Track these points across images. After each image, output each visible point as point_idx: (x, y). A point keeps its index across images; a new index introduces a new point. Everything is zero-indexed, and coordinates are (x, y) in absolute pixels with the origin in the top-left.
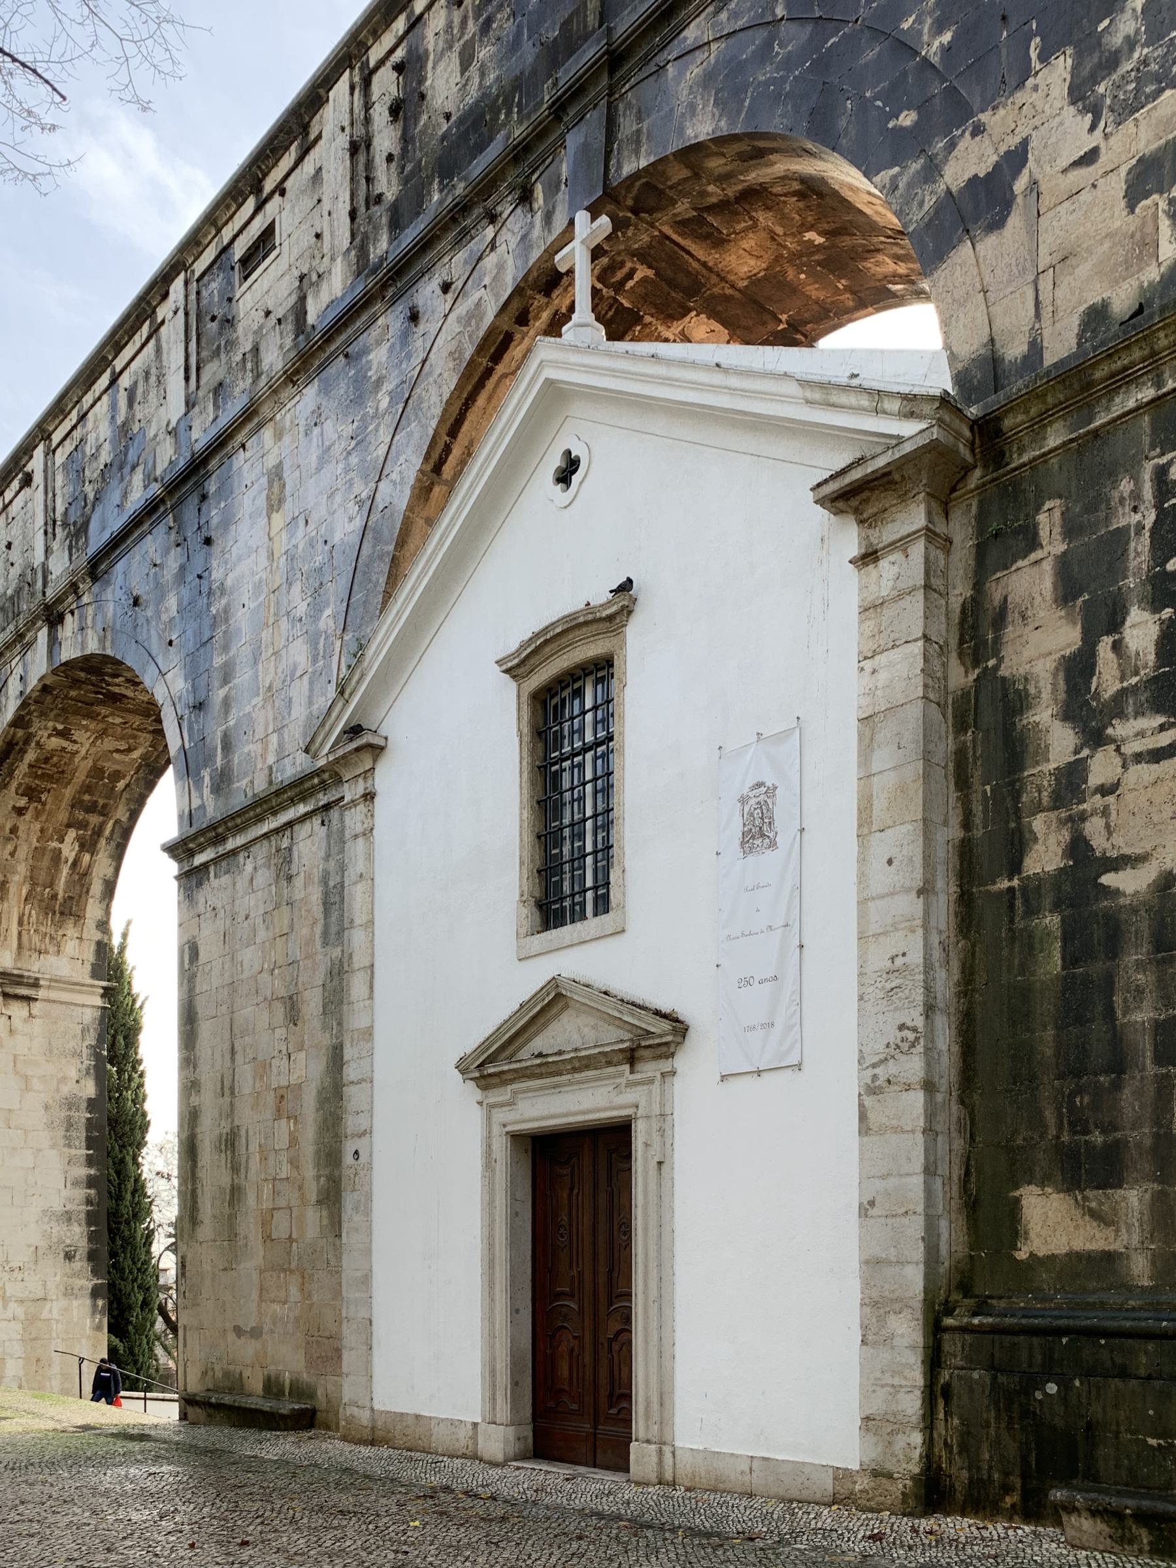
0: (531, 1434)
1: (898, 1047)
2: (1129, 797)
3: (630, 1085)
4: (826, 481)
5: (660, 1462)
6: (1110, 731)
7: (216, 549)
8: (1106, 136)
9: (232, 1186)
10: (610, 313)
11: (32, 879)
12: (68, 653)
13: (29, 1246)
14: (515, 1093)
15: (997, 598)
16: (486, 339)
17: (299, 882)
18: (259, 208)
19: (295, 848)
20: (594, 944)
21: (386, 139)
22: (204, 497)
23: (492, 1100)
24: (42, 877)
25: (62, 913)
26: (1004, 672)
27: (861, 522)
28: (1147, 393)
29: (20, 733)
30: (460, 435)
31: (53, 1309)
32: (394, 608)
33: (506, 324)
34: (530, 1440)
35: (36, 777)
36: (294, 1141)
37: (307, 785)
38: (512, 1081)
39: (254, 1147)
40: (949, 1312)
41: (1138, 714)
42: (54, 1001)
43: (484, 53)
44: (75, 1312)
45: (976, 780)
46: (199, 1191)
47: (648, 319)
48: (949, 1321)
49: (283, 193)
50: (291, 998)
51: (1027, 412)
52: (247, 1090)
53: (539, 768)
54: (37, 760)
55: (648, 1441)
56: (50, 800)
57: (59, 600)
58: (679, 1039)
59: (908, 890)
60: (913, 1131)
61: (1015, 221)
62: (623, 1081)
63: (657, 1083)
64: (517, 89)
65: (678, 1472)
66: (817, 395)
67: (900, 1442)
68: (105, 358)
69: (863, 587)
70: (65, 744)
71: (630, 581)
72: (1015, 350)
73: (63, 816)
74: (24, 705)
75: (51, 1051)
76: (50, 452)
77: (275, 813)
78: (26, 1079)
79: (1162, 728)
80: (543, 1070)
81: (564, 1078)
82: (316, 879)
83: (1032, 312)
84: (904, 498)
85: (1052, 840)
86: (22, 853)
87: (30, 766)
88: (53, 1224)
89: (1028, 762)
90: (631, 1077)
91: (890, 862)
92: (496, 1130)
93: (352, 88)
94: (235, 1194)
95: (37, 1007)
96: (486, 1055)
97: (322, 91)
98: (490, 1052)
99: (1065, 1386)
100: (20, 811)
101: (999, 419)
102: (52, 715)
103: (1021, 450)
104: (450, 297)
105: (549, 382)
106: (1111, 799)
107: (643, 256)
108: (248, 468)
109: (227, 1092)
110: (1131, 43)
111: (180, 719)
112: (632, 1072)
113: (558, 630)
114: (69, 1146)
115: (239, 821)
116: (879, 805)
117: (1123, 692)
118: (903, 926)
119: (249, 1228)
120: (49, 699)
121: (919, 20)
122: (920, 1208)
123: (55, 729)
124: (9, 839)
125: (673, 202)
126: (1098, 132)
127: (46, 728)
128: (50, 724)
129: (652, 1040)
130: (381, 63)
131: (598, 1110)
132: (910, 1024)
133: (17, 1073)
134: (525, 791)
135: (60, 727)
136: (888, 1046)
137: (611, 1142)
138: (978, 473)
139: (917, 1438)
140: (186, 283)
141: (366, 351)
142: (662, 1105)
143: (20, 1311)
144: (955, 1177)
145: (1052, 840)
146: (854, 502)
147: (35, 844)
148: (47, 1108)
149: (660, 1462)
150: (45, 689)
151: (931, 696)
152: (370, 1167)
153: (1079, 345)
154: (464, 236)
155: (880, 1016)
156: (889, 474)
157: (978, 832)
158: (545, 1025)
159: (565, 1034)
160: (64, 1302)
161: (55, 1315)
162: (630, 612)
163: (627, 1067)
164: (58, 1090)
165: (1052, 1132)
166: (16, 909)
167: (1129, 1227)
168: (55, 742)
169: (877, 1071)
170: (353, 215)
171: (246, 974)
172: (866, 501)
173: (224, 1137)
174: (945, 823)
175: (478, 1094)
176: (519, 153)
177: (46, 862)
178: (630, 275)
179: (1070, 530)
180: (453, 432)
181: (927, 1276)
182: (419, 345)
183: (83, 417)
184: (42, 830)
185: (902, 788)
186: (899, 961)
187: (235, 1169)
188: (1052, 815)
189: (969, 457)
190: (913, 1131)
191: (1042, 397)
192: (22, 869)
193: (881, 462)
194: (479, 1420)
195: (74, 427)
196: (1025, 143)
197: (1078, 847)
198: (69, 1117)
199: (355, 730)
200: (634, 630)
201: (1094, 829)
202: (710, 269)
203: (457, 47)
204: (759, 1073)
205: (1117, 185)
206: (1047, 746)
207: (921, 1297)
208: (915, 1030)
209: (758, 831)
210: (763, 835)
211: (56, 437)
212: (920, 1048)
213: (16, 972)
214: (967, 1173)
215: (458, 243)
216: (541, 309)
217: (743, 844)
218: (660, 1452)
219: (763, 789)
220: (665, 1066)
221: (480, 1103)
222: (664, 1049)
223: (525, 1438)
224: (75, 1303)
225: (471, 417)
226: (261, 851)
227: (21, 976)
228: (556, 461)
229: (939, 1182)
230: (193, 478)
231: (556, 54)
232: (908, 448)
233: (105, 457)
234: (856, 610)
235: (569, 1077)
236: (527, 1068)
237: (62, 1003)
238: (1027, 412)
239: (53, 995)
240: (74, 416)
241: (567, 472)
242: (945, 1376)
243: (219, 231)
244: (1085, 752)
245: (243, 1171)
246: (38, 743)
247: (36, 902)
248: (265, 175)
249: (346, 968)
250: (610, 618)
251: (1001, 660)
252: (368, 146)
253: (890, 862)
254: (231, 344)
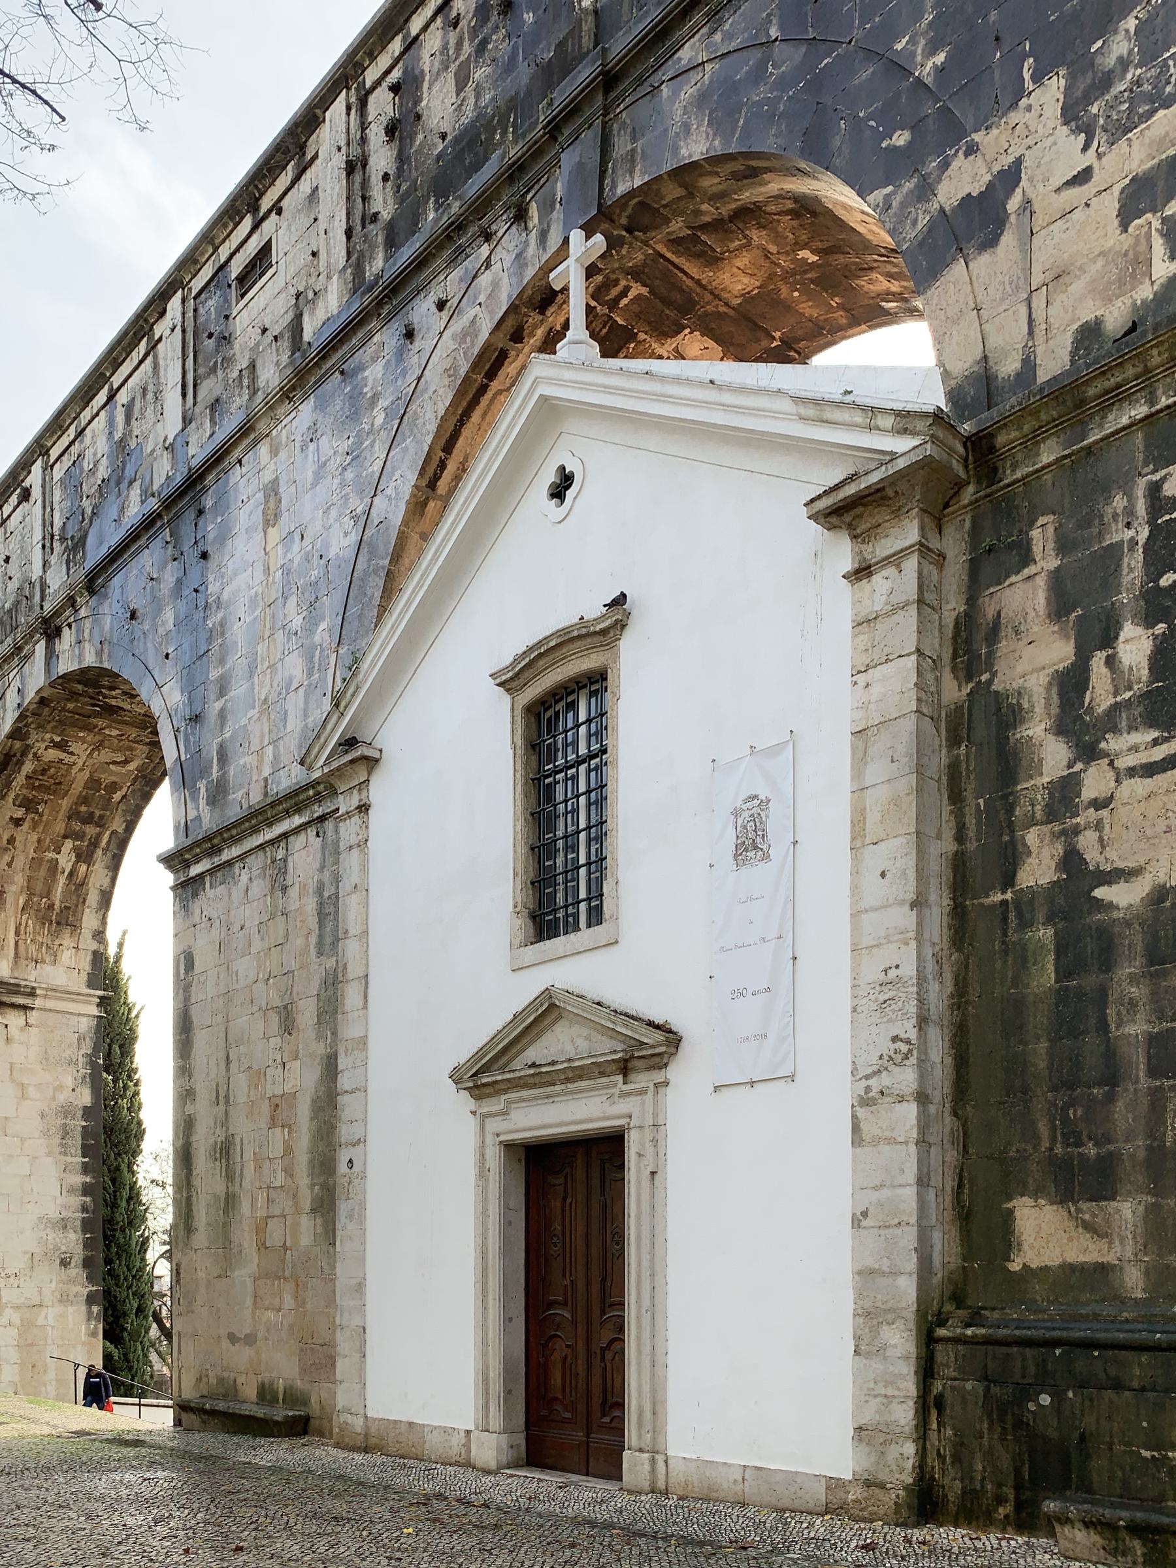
0: (523, 1443)
1: (891, 1058)
2: (1122, 811)
3: (623, 1095)
4: (819, 497)
5: (653, 1470)
6: (1103, 745)
7: (212, 563)
8: (1100, 156)
9: (227, 1193)
10: (604, 331)
11: (29, 889)
12: (66, 665)
13: (25, 1253)
14: (508, 1102)
15: (990, 613)
16: (480, 356)
17: (293, 892)
18: (256, 227)
19: (290, 859)
20: (603, 950)
21: (382, 159)
22: (201, 512)
23: (485, 1110)
24: (39, 886)
25: (58, 923)
26: (997, 686)
27: (855, 537)
28: (1140, 410)
29: (18, 744)
30: (455, 451)
31: (49, 1316)
32: (390, 621)
33: (502, 342)
34: (523, 1449)
35: (34, 788)
36: (288, 1150)
37: (301, 797)
38: (505, 1091)
39: (248, 1155)
40: (942, 1323)
41: (1132, 728)
42: (50, 1010)
43: (479, 74)
44: (70, 1318)
45: (969, 794)
47: (642, 336)
48: (942, 1332)
49: (279, 213)
50: (285, 1007)
51: (1020, 428)
52: (241, 1099)
53: (533, 780)
54: (35, 771)
55: (641, 1450)
56: (47, 812)
57: (57, 613)
58: (672, 1050)
59: (901, 903)
60: (906, 1143)
61: (1008, 240)
62: (616, 1091)
63: (650, 1094)
64: (513, 108)
65: (671, 1481)
66: (811, 412)
67: (893, 1452)
68: (102, 374)
69: (857, 602)
70: (62, 755)
71: (623, 596)
72: (1008, 367)
73: (60, 827)
74: (21, 717)
75: (47, 1059)
76: (49, 467)
77: (270, 825)
78: (23, 1087)
79: (1156, 742)
80: (537, 1080)
81: (557, 1088)
82: (311, 891)
83: (1025, 330)
84: (897, 513)
85: (1046, 852)
86: (20, 862)
87: (28, 777)
88: (48, 1231)
89: (1022, 775)
90: (625, 1087)
91: (883, 875)
92: (490, 1139)
93: (349, 108)
94: (230, 1202)
95: (33, 1016)
96: (479, 1065)
97: (318, 112)
98: (484, 1061)
99: (1058, 1397)
100: (17, 822)
101: (992, 436)
102: (49, 727)
103: (1014, 467)
104: (445, 314)
105: (544, 399)
106: (1104, 813)
107: (637, 274)
108: (244, 483)
109: (222, 1101)
110: (1124, 64)
111: (177, 731)
112: (625, 1083)
113: (552, 644)
114: (65, 1154)
115: (234, 832)
116: (873, 817)
117: (1116, 706)
118: (895, 938)
120: (46, 711)
121: (913, 41)
122: (913, 1220)
123: (52, 741)
124: (6, 849)
125: (668, 221)
126: (1092, 151)
127: (43, 740)
128: (48, 736)
129: (645, 1050)
130: (377, 83)
131: (591, 1120)
132: (903, 1036)
133: (13, 1081)
134: (519, 803)
135: (57, 739)
136: (881, 1057)
137: (605, 1151)
138: (971, 489)
139: (910, 1449)
140: (183, 301)
141: (361, 368)
142: (655, 1115)
143: (16, 1317)
144: (948, 1189)
145: (1046, 852)
146: (848, 518)
147: (32, 854)
148: (43, 1116)
149: (653, 1470)
150: (42, 701)
151: (925, 711)
152: (363, 1176)
153: (1072, 362)
154: (460, 254)
155: (874, 1029)
156: (883, 488)
157: (972, 846)
158: (539, 1035)
159: (560, 1044)
160: (59, 1309)
161: (51, 1321)
162: (623, 627)
163: (620, 1078)
164: (54, 1099)
165: (1046, 1144)
166: (13, 919)
167: (1123, 1240)
168: (53, 754)
169: (870, 1082)
170: (349, 233)
171: (242, 984)
172: (860, 516)
173: (219, 1144)
174: (939, 837)
175: (472, 1104)
176: (515, 172)
177: (43, 872)
178: (624, 294)
179: (1064, 546)
180: (448, 448)
181: (920, 1288)
182: (414, 362)
183: (80, 433)
184: (39, 841)
185: (896, 802)
186: (892, 974)
187: (230, 1176)
188: (1046, 829)
189: (962, 474)
190: (906, 1143)
191: (1035, 413)
192: (19, 879)
193: (874, 478)
194: (472, 1428)
195: (72, 443)
196: (1018, 162)
197: (1071, 861)
198: (65, 1126)
199: (350, 743)
200: (628, 644)
201: (1087, 843)
202: (704, 287)
203: (453, 67)
204: (752, 1084)
205: (1110, 204)
206: (1041, 760)
207: (914, 1308)
208: (908, 1042)
209: (751, 844)
210: (756, 848)
211: (54, 453)
212: (913, 1060)
213: (12, 981)
214: (960, 1185)
215: (453, 261)
216: (536, 326)
217: (736, 856)
218: (653, 1461)
219: (757, 802)
220: (658, 1076)
221: (474, 1113)
222: (657, 1060)
223: (518, 1446)
224: (71, 1309)
225: (466, 432)
226: (256, 862)
227: (18, 985)
228: (549, 477)
229: (932, 1194)
230: (190, 493)
231: (551, 74)
232: (901, 464)
233: (103, 472)
234: (850, 625)
235: (562, 1087)
236: (520, 1078)
237: (58, 1012)
238: (1020, 428)
239: (50, 1004)
240: (72, 432)
241: (561, 487)
242: (938, 1386)
243: (216, 249)
244: (1079, 766)
245: (237, 1180)
246: (35, 754)
247: (32, 912)
248: (262, 194)
249: (340, 978)
250: (603, 632)
251: (994, 674)
252: (365, 165)
253: (883, 875)
254: (228, 361)
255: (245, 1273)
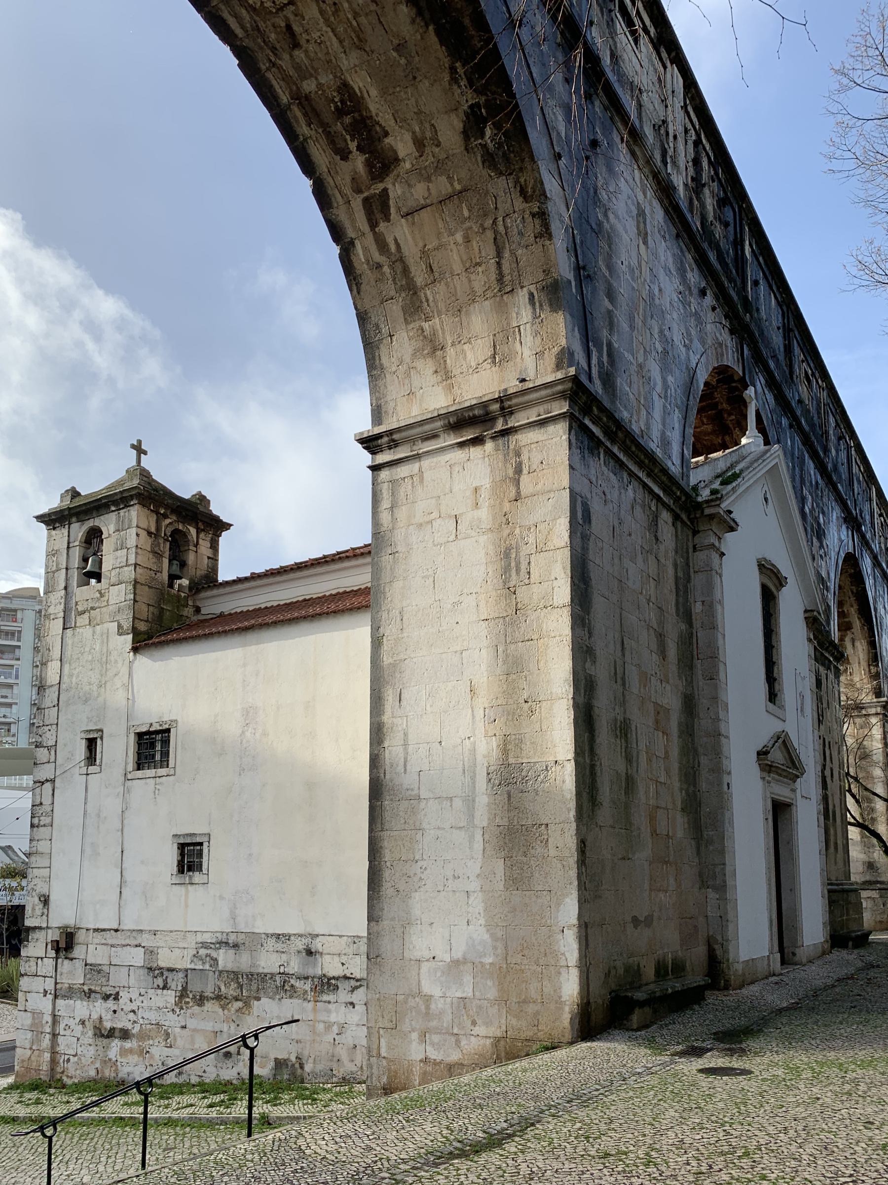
46: (598, 769)
94: (629, 784)
119: (640, 820)
187: (629, 759)
245: (635, 765)
255: (642, 856)
